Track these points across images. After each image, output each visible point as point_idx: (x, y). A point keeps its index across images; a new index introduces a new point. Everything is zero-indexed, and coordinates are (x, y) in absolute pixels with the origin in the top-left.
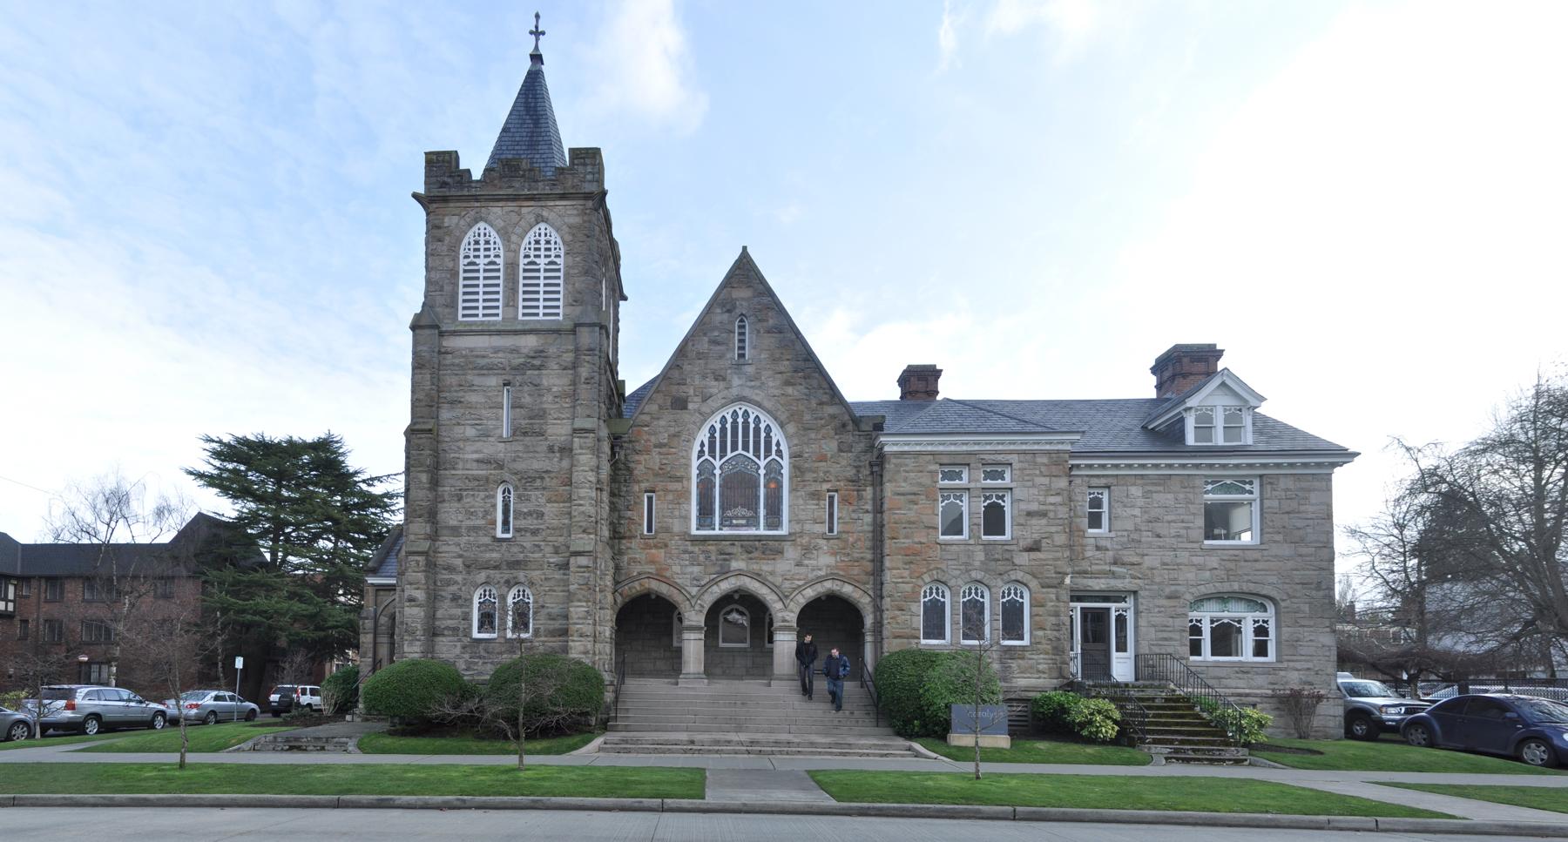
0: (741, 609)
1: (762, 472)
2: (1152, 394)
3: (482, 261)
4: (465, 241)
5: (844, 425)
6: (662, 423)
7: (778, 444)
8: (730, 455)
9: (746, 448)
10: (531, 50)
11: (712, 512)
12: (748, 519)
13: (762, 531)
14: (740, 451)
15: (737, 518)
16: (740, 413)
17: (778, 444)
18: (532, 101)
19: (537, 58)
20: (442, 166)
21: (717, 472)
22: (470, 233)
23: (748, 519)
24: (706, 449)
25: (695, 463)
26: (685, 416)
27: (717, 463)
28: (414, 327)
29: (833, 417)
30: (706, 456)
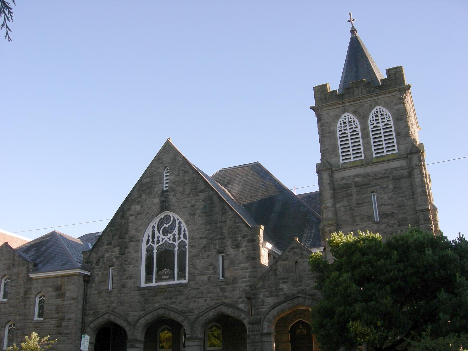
0: (218, 325)
1: (176, 249)
2: (315, 188)
3: (349, 132)
4: (371, 116)
7: (184, 231)
10: (350, 28)
11: (152, 274)
12: (169, 274)
13: (176, 282)
15: (164, 274)
17: (184, 231)
18: (356, 55)
19: (353, 31)
20: (321, 92)
21: (155, 251)
22: (372, 112)
23: (169, 274)
24: (150, 238)
25: (144, 247)
27: (155, 246)
28: (318, 171)
30: (150, 243)
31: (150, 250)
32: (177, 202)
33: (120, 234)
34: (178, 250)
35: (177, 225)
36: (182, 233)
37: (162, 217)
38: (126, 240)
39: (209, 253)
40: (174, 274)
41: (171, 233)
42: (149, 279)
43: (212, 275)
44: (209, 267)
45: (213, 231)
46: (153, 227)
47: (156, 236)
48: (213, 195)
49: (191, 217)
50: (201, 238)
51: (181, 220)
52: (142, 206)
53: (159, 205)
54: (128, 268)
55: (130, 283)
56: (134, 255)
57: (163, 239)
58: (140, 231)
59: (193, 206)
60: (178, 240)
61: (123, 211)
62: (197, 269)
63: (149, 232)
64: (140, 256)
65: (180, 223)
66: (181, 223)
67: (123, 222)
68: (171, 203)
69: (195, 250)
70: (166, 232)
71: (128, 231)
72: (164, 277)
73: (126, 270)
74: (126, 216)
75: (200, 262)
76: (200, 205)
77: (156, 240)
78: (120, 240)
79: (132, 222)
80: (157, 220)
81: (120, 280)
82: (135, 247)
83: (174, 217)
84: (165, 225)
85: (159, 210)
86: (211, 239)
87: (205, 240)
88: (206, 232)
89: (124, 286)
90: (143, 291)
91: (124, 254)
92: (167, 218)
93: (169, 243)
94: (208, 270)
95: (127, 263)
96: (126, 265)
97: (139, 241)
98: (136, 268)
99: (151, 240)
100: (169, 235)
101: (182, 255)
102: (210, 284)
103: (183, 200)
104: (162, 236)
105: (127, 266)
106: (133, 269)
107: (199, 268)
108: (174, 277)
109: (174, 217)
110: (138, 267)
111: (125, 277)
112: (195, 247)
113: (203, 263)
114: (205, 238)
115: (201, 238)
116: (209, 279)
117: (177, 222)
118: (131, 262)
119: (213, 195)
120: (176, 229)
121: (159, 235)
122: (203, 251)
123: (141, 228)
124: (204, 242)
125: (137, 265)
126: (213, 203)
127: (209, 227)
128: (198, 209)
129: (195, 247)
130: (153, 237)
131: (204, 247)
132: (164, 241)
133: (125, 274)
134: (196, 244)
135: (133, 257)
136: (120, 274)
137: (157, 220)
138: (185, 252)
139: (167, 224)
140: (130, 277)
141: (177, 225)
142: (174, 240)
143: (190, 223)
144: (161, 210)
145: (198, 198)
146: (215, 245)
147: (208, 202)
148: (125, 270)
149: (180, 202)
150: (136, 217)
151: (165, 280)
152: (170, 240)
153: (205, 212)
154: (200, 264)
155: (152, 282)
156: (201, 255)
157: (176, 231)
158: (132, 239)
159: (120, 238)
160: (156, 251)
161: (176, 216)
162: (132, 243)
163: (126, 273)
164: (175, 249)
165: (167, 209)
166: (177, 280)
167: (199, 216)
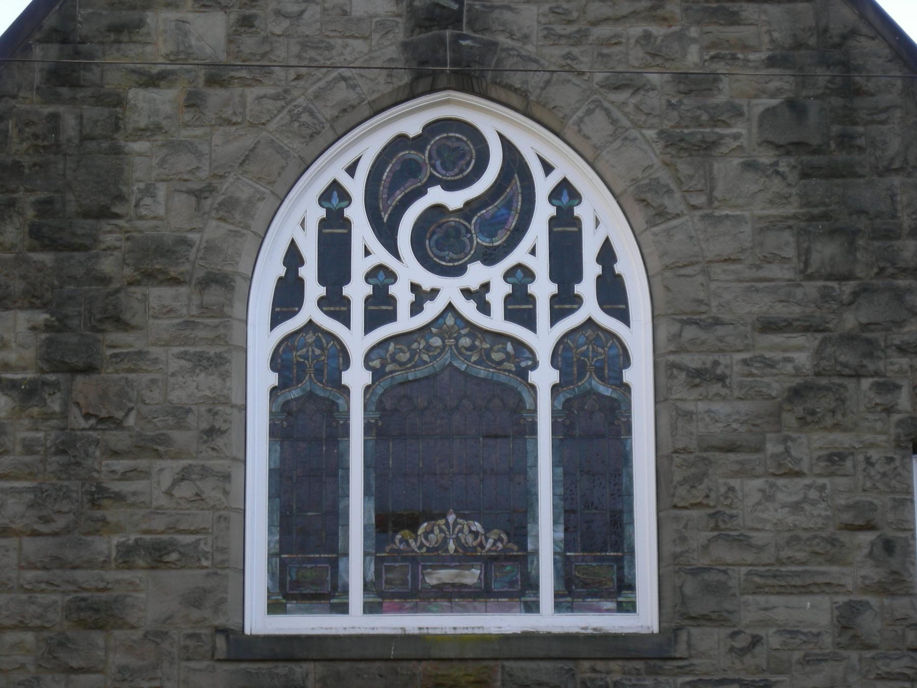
1: (544, 377)
2: (247, 631)
12: (490, 561)
13: (548, 619)
17: (607, 255)
21: (357, 378)
24: (309, 272)
25: (261, 339)
30: (310, 310)
31: (307, 365)
32: (550, 35)
33: (45, 207)
34: (555, 389)
35: (544, 211)
36: (591, 269)
37: (413, 127)
38: (107, 265)
39: (844, 440)
40: (525, 559)
41: (490, 257)
42: (306, 575)
43: (873, 600)
44: (845, 537)
45: (865, 290)
46: (324, 198)
47: (360, 266)
48: (853, 33)
49: (684, 167)
50: (769, 326)
51: (571, 167)
52: (246, 22)
53: (400, 35)
54: (125, 476)
55: (152, 598)
56: (190, 388)
57: (421, 297)
58: (229, 205)
59: (695, 84)
60: (556, 316)
61: (63, 36)
62: (742, 541)
63: (298, 221)
64: (236, 400)
65: (565, 193)
66: (576, 196)
67: (70, 123)
68: (502, 39)
69: (722, 408)
70: (442, 244)
71: (121, 198)
72: (444, 575)
73: (119, 497)
74: (93, 76)
75: (768, 497)
76: (752, 90)
77: (357, 291)
78: (46, 258)
79: (156, 129)
80: (369, 143)
81: (59, 563)
82: (189, 324)
83: (508, 147)
84: (436, 195)
85: (405, 78)
86: (849, 339)
87: (799, 339)
88: (812, 288)
89: (97, 614)
90: (282, 669)
91: (89, 369)
92: (455, 151)
93: (475, 330)
94: (832, 561)
95: (117, 439)
96: (116, 454)
97: (223, 285)
98: (209, 488)
99: (314, 290)
100: (477, 274)
101: (593, 426)
102: (854, 655)
103: (605, 31)
104: (409, 271)
105: (121, 465)
106: (185, 490)
107: (758, 538)
108: (532, 585)
109: (508, 147)
110: (227, 477)
111: (106, 545)
112: (721, 379)
113: (796, 507)
114: (806, 329)
115: (769, 326)
116: (847, 619)
117: (543, 186)
118: (164, 440)
119: (853, 33)
120: (538, 232)
121: (381, 256)
122: (789, 419)
123: (240, 187)
124: (799, 354)
125: (217, 464)
126: (858, 92)
127: (826, 251)
128: (737, 112)
129: (721, 379)
130: (335, 266)
131: (796, 393)
132: (432, 310)
133: (102, 526)
134: (732, 363)
135: (178, 396)
136: (61, 522)
137: (369, 143)
138: (616, 413)
139: (450, 186)
140: (158, 555)
141: (544, 211)
142: (520, 308)
143: (674, 203)
144: (418, 76)
145: (732, 33)
146: (887, 387)
147: (822, 76)
148: (98, 496)
149: (580, 38)
150: (193, 101)
151: (452, 596)
152: (484, 308)
153: (798, 145)
154: (768, 507)
155: (343, 609)
156: (772, 448)
157: (534, 248)
158: (157, 261)
159: (41, 237)
160: (367, 378)
161: (532, 141)
162: (160, 295)
163: (114, 513)
164: (534, 377)
165: (469, 80)
166: (369, 608)
167: (750, 166)
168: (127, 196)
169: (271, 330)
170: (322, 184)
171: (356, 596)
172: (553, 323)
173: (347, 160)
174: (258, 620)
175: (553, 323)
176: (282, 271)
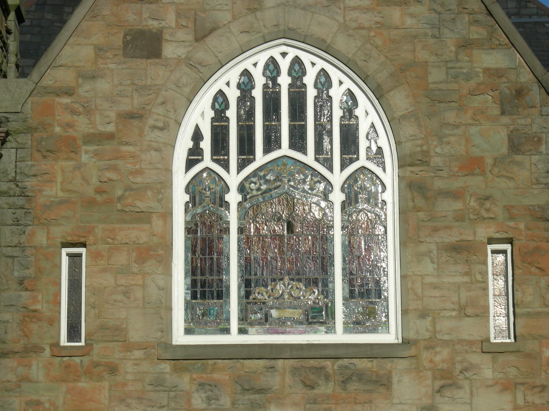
2: (174, 343)
5: (520, 93)
6: (103, 86)
8: (261, 158)
9: (298, 141)
14: (285, 149)
16: (284, 64)
21: (233, 198)
24: (206, 145)
25: (180, 179)
26: (154, 72)
29: (496, 73)
30: (207, 162)
168: (16, 7)
169: (332, 173)
170: (213, 91)
171: (234, 325)
172: (228, 172)
173: (224, 79)
174: (180, 337)
175: (228, 172)
176: (191, 144)
